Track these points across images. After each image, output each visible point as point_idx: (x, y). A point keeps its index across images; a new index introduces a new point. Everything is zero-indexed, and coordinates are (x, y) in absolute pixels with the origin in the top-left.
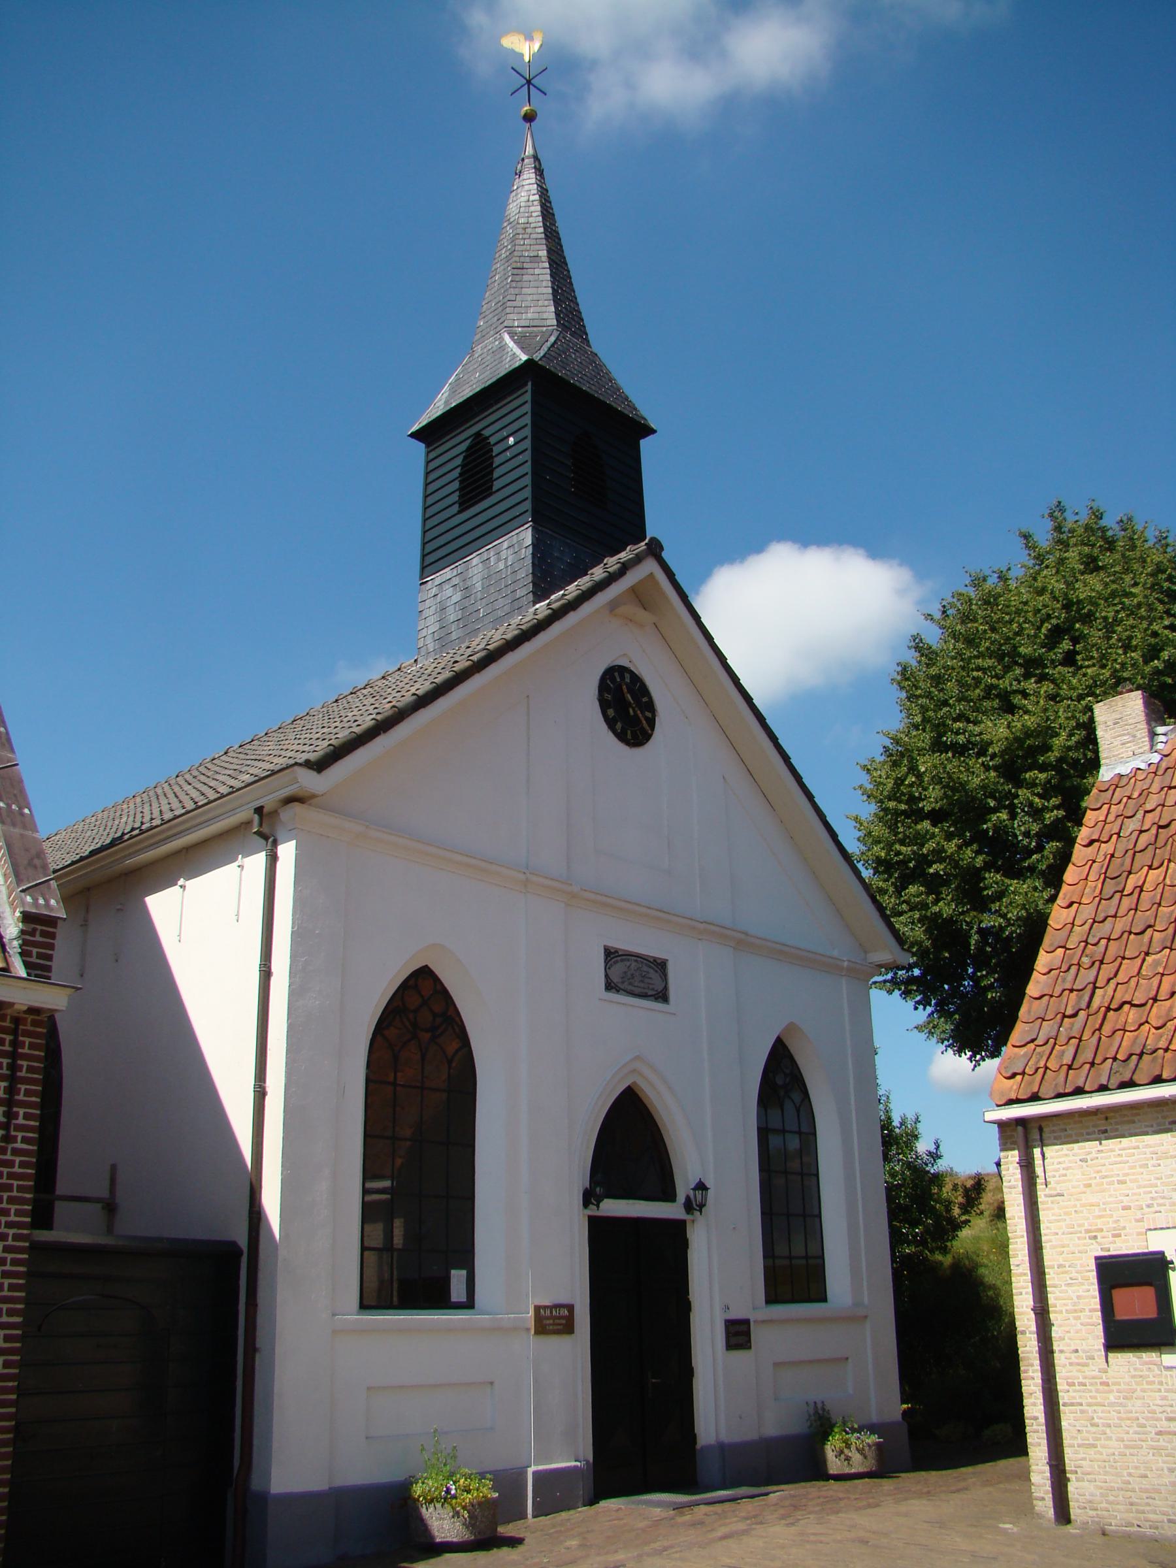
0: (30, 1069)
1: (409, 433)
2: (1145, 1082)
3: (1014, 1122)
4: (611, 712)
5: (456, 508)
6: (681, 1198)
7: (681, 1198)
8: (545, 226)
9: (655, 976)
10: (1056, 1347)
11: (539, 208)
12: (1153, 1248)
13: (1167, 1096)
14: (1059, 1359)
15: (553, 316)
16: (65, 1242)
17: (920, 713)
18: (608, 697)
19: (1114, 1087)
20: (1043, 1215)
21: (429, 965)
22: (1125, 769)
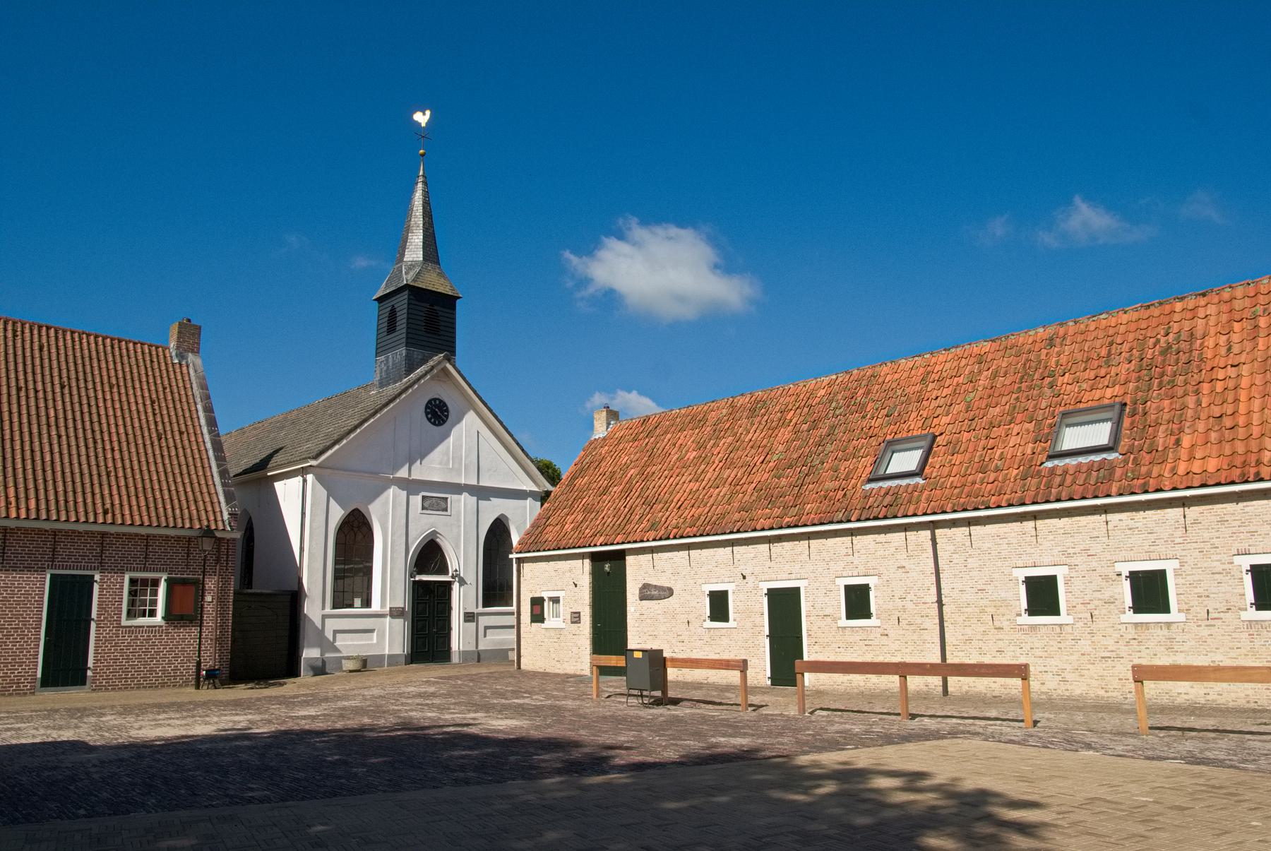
0: (226, 659)
1: (374, 298)
2: (1212, 483)
3: (1037, 517)
4: (430, 416)
5: (385, 334)
6: (450, 574)
7: (450, 574)
8: (405, 252)
9: (443, 504)
10: (522, 622)
11: (422, 208)
12: (542, 596)
13: (1237, 491)
14: (522, 625)
15: (422, 256)
16: (741, 678)
17: (204, 602)
18: (428, 410)
19: (921, 514)
20: (522, 586)
21: (359, 508)
22: (597, 437)
